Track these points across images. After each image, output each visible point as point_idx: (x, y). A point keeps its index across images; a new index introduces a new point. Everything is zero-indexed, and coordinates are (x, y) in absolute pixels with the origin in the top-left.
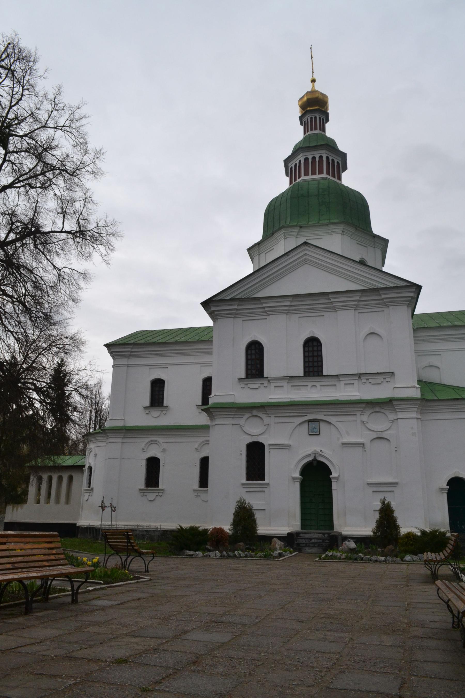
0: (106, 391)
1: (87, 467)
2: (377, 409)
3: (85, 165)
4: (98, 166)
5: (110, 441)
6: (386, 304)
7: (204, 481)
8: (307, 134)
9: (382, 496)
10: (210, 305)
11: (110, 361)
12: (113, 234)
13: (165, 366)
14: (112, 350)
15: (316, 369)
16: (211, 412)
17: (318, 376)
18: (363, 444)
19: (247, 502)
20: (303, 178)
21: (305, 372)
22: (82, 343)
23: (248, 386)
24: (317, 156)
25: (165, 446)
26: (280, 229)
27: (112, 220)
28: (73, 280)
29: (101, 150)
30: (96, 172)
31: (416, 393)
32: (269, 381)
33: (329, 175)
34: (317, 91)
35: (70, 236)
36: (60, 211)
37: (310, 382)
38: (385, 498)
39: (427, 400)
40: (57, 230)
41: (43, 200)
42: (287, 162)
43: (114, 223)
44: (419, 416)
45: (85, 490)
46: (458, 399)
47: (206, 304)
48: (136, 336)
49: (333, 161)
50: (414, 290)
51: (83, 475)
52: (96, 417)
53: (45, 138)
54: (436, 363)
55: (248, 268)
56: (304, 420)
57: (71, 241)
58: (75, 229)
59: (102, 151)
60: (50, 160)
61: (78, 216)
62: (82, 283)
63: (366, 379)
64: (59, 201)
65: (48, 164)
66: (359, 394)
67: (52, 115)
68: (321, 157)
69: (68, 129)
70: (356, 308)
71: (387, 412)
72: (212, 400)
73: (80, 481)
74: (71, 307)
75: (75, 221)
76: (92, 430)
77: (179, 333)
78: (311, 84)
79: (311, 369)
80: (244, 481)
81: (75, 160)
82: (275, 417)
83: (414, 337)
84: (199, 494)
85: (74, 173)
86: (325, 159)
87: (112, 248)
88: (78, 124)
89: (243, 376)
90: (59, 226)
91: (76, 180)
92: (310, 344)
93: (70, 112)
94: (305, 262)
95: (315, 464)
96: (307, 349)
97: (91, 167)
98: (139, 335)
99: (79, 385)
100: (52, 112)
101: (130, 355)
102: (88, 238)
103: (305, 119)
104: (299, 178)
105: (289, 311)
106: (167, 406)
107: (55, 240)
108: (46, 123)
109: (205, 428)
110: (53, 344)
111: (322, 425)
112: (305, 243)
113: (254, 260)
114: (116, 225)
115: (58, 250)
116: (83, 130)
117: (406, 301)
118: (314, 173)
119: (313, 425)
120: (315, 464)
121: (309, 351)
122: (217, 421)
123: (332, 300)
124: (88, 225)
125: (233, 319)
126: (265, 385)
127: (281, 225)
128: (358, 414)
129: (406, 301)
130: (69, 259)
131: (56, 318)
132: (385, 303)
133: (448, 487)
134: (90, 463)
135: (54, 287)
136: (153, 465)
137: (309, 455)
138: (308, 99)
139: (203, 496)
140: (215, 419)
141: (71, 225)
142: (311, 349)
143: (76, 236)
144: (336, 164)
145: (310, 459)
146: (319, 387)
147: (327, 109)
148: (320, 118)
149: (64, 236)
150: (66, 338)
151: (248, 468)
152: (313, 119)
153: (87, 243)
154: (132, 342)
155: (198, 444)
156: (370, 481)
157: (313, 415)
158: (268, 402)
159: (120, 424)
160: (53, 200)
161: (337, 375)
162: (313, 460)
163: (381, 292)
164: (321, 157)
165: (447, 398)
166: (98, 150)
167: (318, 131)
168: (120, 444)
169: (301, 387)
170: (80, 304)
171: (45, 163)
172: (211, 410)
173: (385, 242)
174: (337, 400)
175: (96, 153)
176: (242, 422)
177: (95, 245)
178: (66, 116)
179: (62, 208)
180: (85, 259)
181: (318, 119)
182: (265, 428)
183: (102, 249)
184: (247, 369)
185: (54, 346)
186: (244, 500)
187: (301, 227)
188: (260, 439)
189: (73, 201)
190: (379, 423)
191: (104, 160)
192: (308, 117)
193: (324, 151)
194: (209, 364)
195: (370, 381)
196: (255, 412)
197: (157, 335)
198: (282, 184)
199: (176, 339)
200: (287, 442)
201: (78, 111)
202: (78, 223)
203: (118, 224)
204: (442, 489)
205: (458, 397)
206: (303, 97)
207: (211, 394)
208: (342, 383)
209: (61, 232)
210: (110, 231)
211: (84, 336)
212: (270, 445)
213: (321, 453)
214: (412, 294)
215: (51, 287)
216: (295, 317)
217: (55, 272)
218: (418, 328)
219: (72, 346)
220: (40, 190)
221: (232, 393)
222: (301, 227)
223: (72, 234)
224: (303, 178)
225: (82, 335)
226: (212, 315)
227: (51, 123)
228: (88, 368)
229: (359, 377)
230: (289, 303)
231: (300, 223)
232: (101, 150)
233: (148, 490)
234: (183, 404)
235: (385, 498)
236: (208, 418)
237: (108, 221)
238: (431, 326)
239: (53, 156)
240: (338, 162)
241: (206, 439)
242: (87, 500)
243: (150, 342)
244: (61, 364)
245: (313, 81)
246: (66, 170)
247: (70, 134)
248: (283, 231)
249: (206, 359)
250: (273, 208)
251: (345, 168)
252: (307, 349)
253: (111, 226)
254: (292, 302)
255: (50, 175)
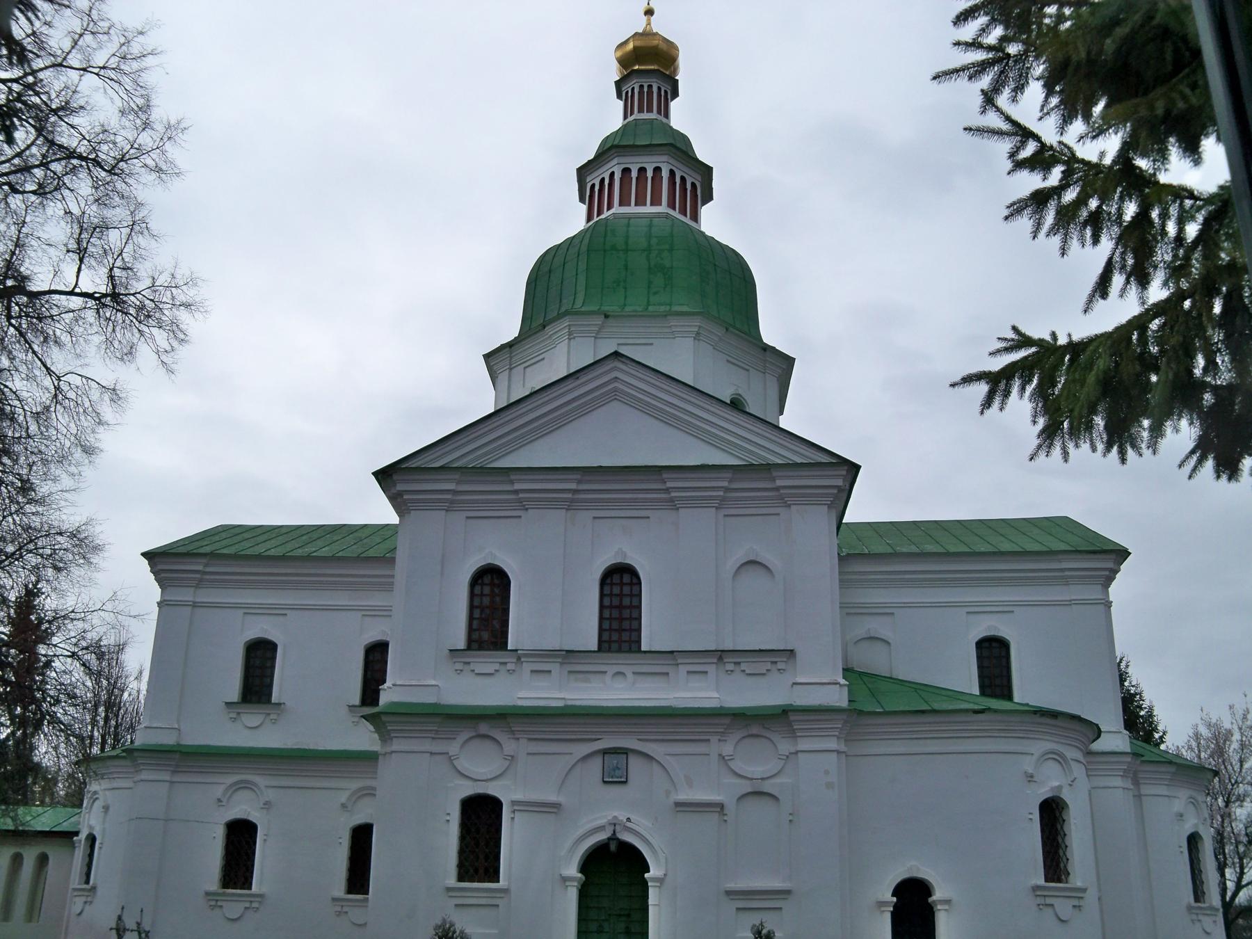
0: (138, 660)
1: (83, 836)
2: (755, 730)
3: (141, 151)
4: (169, 155)
5: (143, 777)
6: (783, 499)
7: (358, 878)
8: (630, 119)
9: (755, 919)
10: (395, 477)
11: (156, 592)
12: (187, 305)
13: (277, 611)
14: (160, 567)
15: (625, 636)
16: (384, 723)
17: (630, 651)
18: (721, 806)
19: (458, 927)
20: (616, 209)
21: (600, 641)
22: (97, 549)
23: (472, 666)
24: (646, 163)
25: (271, 795)
26: (560, 316)
27: (188, 273)
28: (87, 404)
29: (179, 123)
30: (164, 168)
31: (839, 698)
32: (519, 658)
33: (674, 209)
34: (657, 34)
35: (91, 303)
36: (73, 245)
37: (614, 663)
38: (761, 924)
39: (861, 713)
40: (63, 288)
41: (38, 220)
42: (583, 172)
43: (192, 282)
44: (843, 748)
45: (75, 890)
46: (923, 712)
47: (385, 476)
48: (217, 538)
49: (683, 179)
50: (844, 473)
51: (73, 855)
52: (107, 719)
53: (57, 89)
54: (885, 633)
55: (483, 401)
56: (590, 751)
57: (90, 315)
58: (103, 289)
59: (182, 126)
60: (66, 138)
61: (111, 261)
62: (107, 411)
63: (735, 663)
64: (76, 226)
65: (61, 146)
66: (716, 695)
67: (80, 43)
68: (657, 170)
69: (112, 74)
70: (721, 504)
71: (776, 738)
72: (387, 696)
73: (66, 867)
74: (78, 465)
75: (104, 271)
76: (96, 750)
77: (315, 535)
78: (645, 18)
79: (615, 637)
80: (452, 881)
81: (119, 139)
82: (530, 739)
83: (840, 573)
84: (345, 909)
85: (114, 167)
86: (665, 174)
87: (182, 336)
88: (135, 65)
89: (461, 643)
90: (67, 279)
91: (120, 185)
92: (616, 578)
93: (123, 40)
94: (614, 395)
95: (613, 847)
96: (607, 590)
97: (154, 156)
98: (224, 535)
99: (84, 644)
100: (81, 35)
101: (201, 580)
102: (132, 311)
103: (626, 88)
104: (609, 209)
105: (571, 504)
106: (279, 704)
107: (55, 312)
108: (65, 59)
109: (369, 758)
110: (31, 546)
111: (634, 762)
112: (616, 355)
113: (498, 381)
114: (196, 285)
115: (58, 332)
116: (146, 78)
117: (826, 495)
118: (640, 202)
119: (612, 760)
120: (613, 847)
121: (611, 595)
122: (397, 745)
123: (669, 484)
124: (134, 282)
125: (443, 512)
126: (510, 666)
127: (563, 309)
128: (714, 739)
129: (826, 495)
130: (83, 354)
131: (43, 489)
132: (781, 498)
133: (895, 899)
134: (91, 827)
135: (41, 415)
136: (241, 837)
137: (601, 828)
138: (635, 48)
139: (356, 914)
140: (391, 739)
141: (93, 280)
142: (616, 590)
143: (105, 306)
144: (689, 186)
145: (602, 836)
146: (630, 676)
147: (675, 71)
148: (659, 89)
149: (76, 302)
150: (61, 534)
151: (462, 852)
152: (646, 89)
153: (128, 322)
154: (207, 550)
155: (347, 794)
156: (731, 886)
157: (617, 742)
158: (514, 707)
159: (169, 740)
160: (63, 223)
161: (672, 652)
162: (609, 839)
163: (775, 474)
164: (657, 170)
165: (901, 708)
166: (172, 122)
167: (653, 115)
168: (167, 784)
169: (588, 676)
170: (99, 459)
171: (52, 143)
172: (384, 718)
173: (787, 362)
174: (670, 707)
175: (168, 127)
176: (453, 748)
177: (143, 327)
178: (113, 47)
179: (79, 241)
180: (122, 359)
181: (655, 89)
182: (507, 763)
183: (160, 336)
184: (471, 630)
185: (30, 552)
186: (452, 925)
187: (606, 316)
188: (492, 790)
189: (103, 227)
190: (756, 760)
191: (183, 144)
192: (635, 84)
193: (665, 158)
194: (384, 612)
195: (743, 666)
196: (484, 728)
197: (265, 537)
198: (573, 220)
199: (307, 550)
200: (553, 798)
201: (141, 38)
202: (111, 277)
203: (200, 283)
204: (882, 904)
205: (925, 707)
206: (626, 42)
207: (384, 682)
208: (683, 669)
209: (72, 293)
210: (181, 298)
211: (101, 533)
212: (514, 803)
213: (628, 824)
214: (840, 482)
215: (37, 415)
216: (585, 517)
217: (48, 382)
218: (848, 555)
219: (73, 554)
220: (33, 198)
221: (433, 682)
222: (606, 316)
223: (96, 299)
224: (616, 209)
225: (98, 529)
226: (396, 500)
227: (75, 60)
228: (109, 606)
229: (720, 658)
230: (573, 486)
231: (605, 308)
232: (179, 123)
233: (224, 894)
234: (316, 700)
235: (761, 924)
236: (376, 736)
237: (178, 276)
238: (876, 551)
239: (73, 127)
240: (695, 183)
241: (368, 783)
242: (80, 914)
243: (248, 552)
244: (31, 594)
245: (650, 12)
246: (97, 163)
247: (116, 86)
248: (565, 322)
249: (377, 600)
250: (547, 269)
251: (708, 197)
252: (607, 590)
253: (184, 288)
254: (579, 482)
255: (57, 167)
